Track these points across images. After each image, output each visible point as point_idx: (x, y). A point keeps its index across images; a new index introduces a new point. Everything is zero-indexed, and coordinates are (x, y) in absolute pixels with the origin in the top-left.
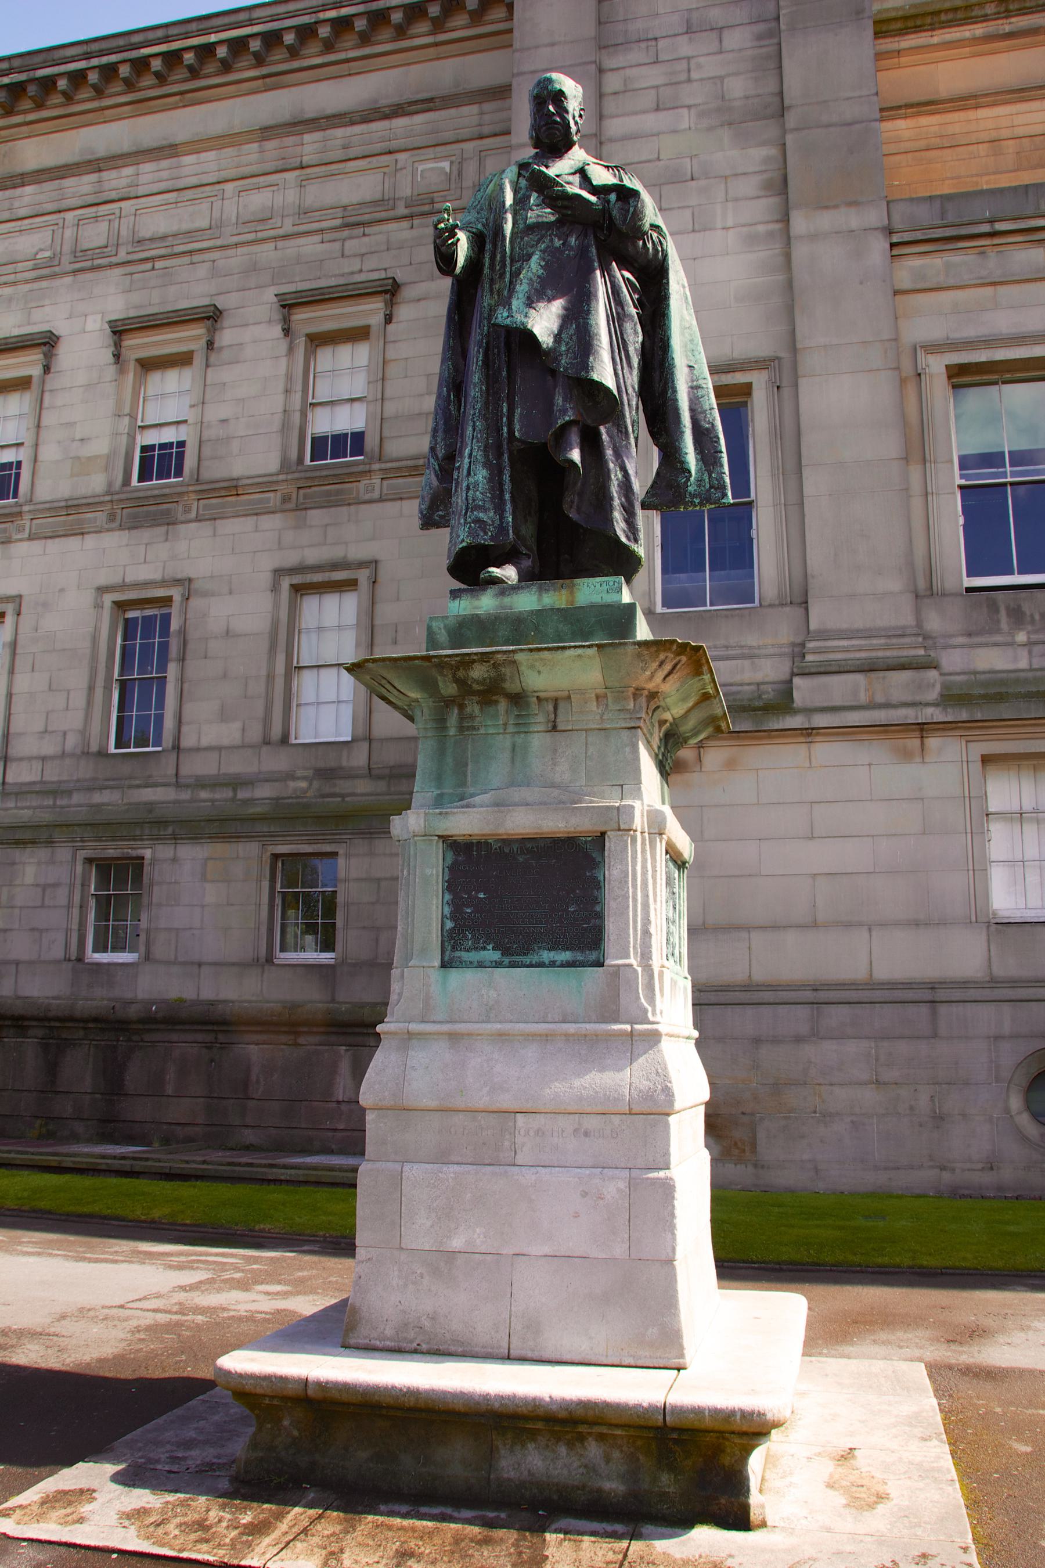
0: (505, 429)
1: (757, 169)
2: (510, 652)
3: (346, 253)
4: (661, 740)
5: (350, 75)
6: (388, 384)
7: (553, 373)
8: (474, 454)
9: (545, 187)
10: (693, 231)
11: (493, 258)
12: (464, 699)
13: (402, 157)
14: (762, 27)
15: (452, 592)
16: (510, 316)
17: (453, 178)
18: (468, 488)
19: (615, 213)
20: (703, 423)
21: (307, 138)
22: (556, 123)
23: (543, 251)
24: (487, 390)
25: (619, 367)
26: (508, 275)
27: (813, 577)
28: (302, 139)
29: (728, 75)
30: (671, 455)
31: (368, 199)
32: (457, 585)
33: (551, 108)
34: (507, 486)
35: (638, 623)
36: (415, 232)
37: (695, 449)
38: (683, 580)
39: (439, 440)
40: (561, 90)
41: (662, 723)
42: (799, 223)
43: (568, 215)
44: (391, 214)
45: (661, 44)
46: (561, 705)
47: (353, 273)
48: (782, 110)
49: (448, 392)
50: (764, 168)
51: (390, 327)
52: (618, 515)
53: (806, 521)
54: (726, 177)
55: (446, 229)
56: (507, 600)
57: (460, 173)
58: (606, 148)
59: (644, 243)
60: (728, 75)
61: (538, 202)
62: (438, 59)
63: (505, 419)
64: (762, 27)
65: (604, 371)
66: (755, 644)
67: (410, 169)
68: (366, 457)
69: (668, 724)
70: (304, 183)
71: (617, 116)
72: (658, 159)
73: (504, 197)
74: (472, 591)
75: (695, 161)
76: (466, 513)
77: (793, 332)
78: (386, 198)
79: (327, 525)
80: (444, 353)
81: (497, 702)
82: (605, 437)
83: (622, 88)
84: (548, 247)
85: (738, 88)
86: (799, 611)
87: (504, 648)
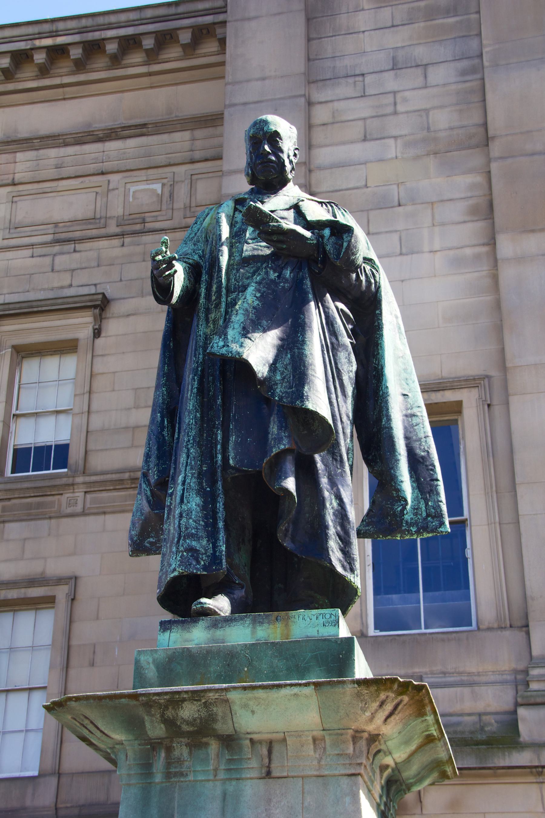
0: (220, 457)
1: (463, 195)
2: (222, 690)
3: (56, 268)
4: (382, 788)
5: (64, 99)
6: (94, 396)
7: (268, 401)
8: (188, 481)
9: (263, 224)
10: (401, 254)
12: (172, 742)
13: (114, 178)
14: (465, 64)
15: (162, 623)
16: (226, 345)
18: (181, 516)
19: (328, 248)
20: (418, 451)
21: (20, 156)
22: (272, 161)
23: (259, 283)
24: (202, 417)
25: (333, 396)
26: (223, 305)
27: (533, 599)
28: (15, 157)
29: (434, 108)
31: (80, 217)
32: (168, 616)
33: (267, 148)
34: (221, 515)
35: (356, 658)
36: (125, 250)
37: (411, 477)
38: (396, 601)
39: (152, 465)
41: (383, 768)
42: (506, 246)
43: (283, 249)
44: (103, 231)
45: (368, 79)
46: (276, 748)
47: (62, 288)
48: (486, 141)
50: (469, 194)
51: (98, 341)
52: (333, 545)
53: (523, 540)
54: (432, 203)
55: (163, 261)
56: (219, 633)
57: (171, 195)
58: (316, 176)
59: (358, 276)
60: (434, 108)
61: (253, 236)
62: (152, 87)
63: (219, 447)
64: (465, 64)
66: (474, 670)
67: (122, 190)
68: (70, 469)
69: (389, 770)
70: (15, 199)
71: (326, 146)
72: (366, 186)
73: (220, 231)
74: (183, 622)
75: (402, 188)
76: (178, 541)
77: (502, 351)
78: (98, 216)
79: (25, 539)
80: (158, 379)
81: (207, 744)
82: (320, 465)
83: (331, 120)
84: (263, 279)
85: (443, 120)
86: (520, 635)
87: (217, 686)
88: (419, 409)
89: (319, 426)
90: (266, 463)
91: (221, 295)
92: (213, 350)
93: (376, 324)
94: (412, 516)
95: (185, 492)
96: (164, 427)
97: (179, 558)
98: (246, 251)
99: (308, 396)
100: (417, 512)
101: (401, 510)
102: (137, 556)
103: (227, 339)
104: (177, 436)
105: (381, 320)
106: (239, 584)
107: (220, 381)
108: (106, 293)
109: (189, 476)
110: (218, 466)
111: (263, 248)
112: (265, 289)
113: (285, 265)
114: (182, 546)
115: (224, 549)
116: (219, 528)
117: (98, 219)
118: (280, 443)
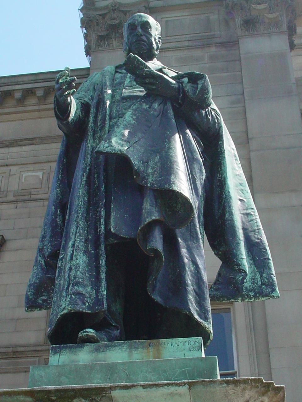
0: (103, 227)
8: (77, 244)
11: (96, 117)
13: (14, 169)
17: (44, 182)
18: (70, 269)
26: (107, 126)
30: (228, 258)
34: (103, 268)
40: (147, 21)
44: (5, 199)
49: (56, 209)
52: (191, 297)
63: (102, 220)
65: (182, 185)
76: (68, 288)
84: (138, 108)
88: (253, 210)
89: (181, 208)
90: (141, 230)
91: (106, 120)
92: (100, 149)
93: (220, 150)
94: (250, 284)
95: (75, 251)
96: (58, 215)
97: (68, 299)
98: (124, 93)
99: (174, 181)
100: (254, 281)
101: (242, 279)
102: (32, 311)
103: (111, 142)
104: (68, 218)
105: (223, 147)
106: (114, 326)
107: (104, 175)
108: (4, 235)
109: (77, 240)
110: (101, 234)
111: (137, 92)
112: (139, 114)
113: (154, 101)
114: (71, 290)
115: (105, 293)
116: (101, 278)
117: (2, 192)
118: (152, 215)
